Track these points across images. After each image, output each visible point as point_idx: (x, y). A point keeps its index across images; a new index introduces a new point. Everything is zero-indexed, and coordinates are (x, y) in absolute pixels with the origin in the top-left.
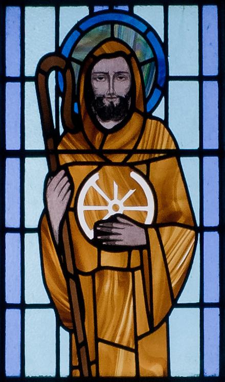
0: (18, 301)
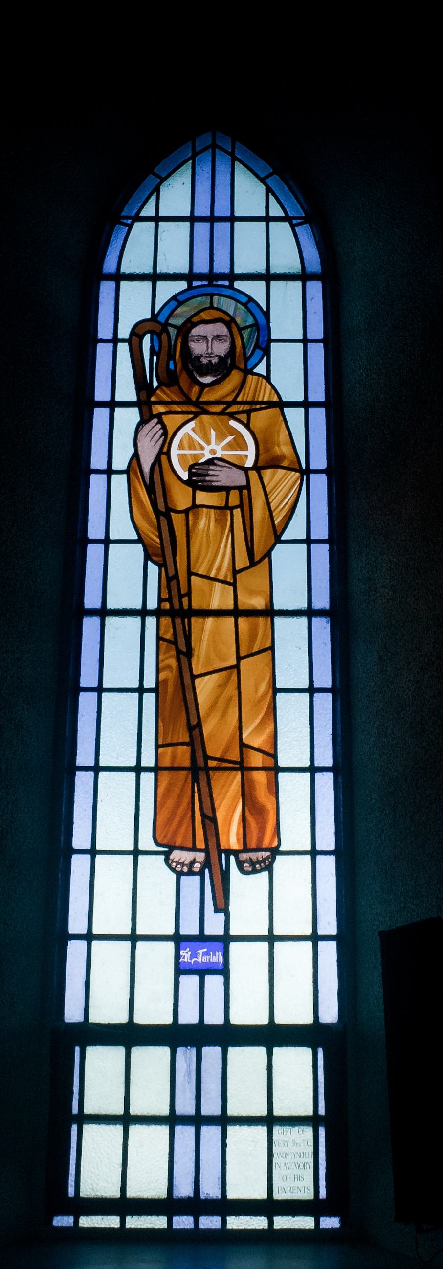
0: (318, 776)
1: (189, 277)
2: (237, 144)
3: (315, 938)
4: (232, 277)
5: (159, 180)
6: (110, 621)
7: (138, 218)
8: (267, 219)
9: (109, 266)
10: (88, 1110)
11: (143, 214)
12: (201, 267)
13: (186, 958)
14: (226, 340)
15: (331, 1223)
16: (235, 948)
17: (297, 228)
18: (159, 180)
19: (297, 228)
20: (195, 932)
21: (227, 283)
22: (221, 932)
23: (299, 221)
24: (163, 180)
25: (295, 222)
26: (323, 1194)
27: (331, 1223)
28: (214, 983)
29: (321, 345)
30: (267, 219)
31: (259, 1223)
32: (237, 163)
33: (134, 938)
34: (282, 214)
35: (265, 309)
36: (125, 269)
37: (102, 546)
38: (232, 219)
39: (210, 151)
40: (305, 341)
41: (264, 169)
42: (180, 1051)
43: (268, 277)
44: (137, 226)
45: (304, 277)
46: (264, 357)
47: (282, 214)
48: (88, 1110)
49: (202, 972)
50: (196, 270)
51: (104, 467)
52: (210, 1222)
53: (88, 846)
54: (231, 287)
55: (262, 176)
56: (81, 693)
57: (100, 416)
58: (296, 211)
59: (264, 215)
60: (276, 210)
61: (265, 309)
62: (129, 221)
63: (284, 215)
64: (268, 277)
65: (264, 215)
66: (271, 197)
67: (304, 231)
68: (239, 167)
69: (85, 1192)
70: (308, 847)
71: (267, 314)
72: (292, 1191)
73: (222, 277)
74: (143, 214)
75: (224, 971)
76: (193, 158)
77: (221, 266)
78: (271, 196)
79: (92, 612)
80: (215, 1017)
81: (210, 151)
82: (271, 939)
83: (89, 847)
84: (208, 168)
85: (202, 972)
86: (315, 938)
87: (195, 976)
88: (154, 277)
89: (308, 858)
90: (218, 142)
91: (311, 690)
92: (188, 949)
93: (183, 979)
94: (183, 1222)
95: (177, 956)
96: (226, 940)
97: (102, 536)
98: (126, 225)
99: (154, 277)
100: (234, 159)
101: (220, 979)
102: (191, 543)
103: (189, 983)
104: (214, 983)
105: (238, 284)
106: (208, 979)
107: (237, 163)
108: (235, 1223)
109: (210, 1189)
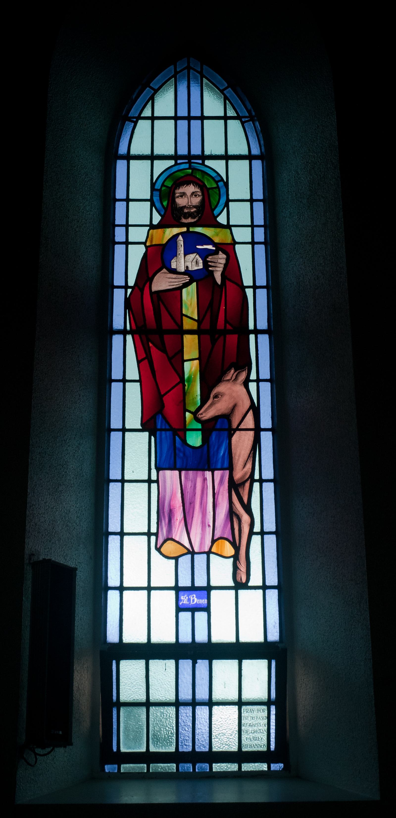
1: (175, 157)
2: (205, 67)
3: (121, 589)
4: (203, 157)
5: (153, 92)
6: (133, 163)
7: (140, 118)
8: (225, 118)
9: (122, 150)
10: (123, 698)
11: (143, 115)
12: (183, 151)
13: (185, 601)
14: (199, 196)
16: (214, 593)
18: (153, 92)
20: (189, 584)
21: (200, 162)
22: (205, 584)
23: (247, 119)
25: (243, 120)
26: (273, 747)
27: (277, 767)
28: (201, 617)
30: (225, 118)
31: (233, 767)
33: (240, 703)
35: (154, 208)
36: (133, 152)
39: (186, 71)
42: (181, 662)
43: (227, 157)
45: (250, 157)
46: (225, 208)
48: (123, 698)
49: (193, 610)
52: (203, 767)
54: (203, 164)
55: (221, 88)
60: (231, 113)
61: (154, 208)
62: (135, 120)
64: (227, 157)
71: (226, 184)
72: (258, 739)
74: (143, 115)
75: (207, 609)
76: (175, 76)
77: (196, 150)
80: (201, 637)
81: (186, 71)
82: (149, 589)
84: (186, 83)
85: (193, 610)
86: (121, 589)
88: (152, 158)
90: (192, 65)
92: (186, 595)
93: (181, 614)
94: (187, 767)
96: (208, 589)
98: (133, 122)
99: (152, 158)
100: (202, 76)
103: (185, 616)
105: (207, 163)
106: (197, 614)
108: (218, 767)
109: (202, 747)
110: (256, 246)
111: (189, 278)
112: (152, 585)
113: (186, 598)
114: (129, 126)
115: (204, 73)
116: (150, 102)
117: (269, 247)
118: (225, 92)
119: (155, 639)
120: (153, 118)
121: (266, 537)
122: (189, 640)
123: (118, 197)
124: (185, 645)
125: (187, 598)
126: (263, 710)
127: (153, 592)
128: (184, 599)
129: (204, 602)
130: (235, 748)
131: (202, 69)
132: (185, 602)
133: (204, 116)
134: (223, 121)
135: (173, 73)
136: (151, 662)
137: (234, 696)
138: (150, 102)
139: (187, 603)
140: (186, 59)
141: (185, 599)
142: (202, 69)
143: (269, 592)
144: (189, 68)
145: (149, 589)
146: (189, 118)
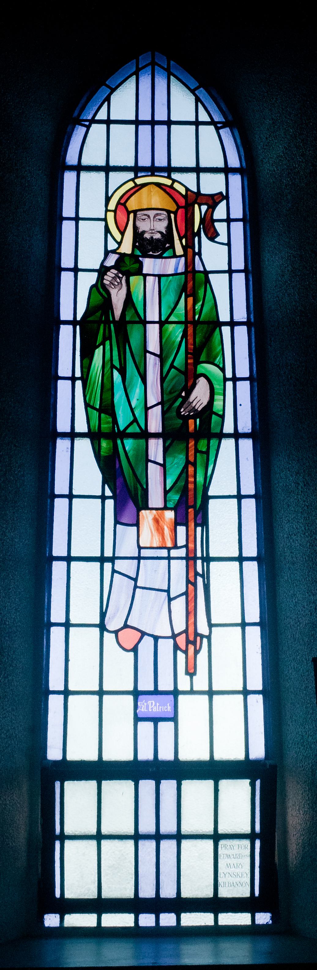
0: (245, 564)
2: (172, 63)
3: (66, 693)
6: (84, 175)
7: (94, 121)
9: (71, 158)
11: (97, 118)
12: (145, 115)
15: (263, 918)
17: (221, 131)
19: (221, 131)
24: (113, 90)
25: (219, 125)
27: (263, 918)
28: (166, 728)
29: (255, 563)
30: (197, 123)
32: (172, 78)
33: (99, 837)
34: (209, 120)
36: (85, 162)
37: (73, 223)
38: (169, 123)
40: (239, 497)
41: (194, 84)
44: (94, 126)
47: (209, 120)
49: (156, 720)
50: (140, 164)
51: (73, 215)
53: (67, 492)
56: (54, 562)
57: (62, 445)
58: (217, 117)
59: (194, 120)
60: (203, 116)
62: (87, 123)
63: (210, 121)
65: (194, 120)
66: (200, 105)
67: (225, 133)
68: (174, 82)
69: (68, 895)
70: (239, 621)
73: (161, 169)
74: (97, 118)
75: (174, 719)
76: (137, 74)
78: (199, 104)
79: (64, 435)
83: (62, 688)
87: (150, 781)
88: (107, 169)
89: (239, 629)
91: (246, 692)
92: (144, 701)
93: (140, 724)
95: (136, 707)
96: (176, 693)
97: (73, 215)
99: (107, 169)
101: (171, 724)
102: (143, 343)
103: (146, 728)
104: (166, 728)
107: (172, 78)
110: (232, 224)
111: (182, 414)
112: (105, 688)
113: (143, 704)
114: (80, 131)
115: (172, 71)
116: (106, 103)
117: (253, 329)
118: (196, 92)
119: (107, 757)
120: (108, 122)
121: (248, 628)
122: (151, 757)
123: (65, 215)
124: (146, 763)
125: (145, 704)
126: (245, 846)
127: (105, 697)
128: (142, 705)
129: (169, 709)
130: (93, 895)
131: (169, 65)
132: (143, 710)
133: (171, 120)
134: (194, 127)
135: (134, 69)
136: (104, 783)
137: (209, 829)
138: (106, 103)
139: (145, 710)
140: (149, 53)
141: (143, 706)
142: (169, 65)
143: (64, 553)
144: (153, 64)
145: (101, 693)
146: (153, 123)
